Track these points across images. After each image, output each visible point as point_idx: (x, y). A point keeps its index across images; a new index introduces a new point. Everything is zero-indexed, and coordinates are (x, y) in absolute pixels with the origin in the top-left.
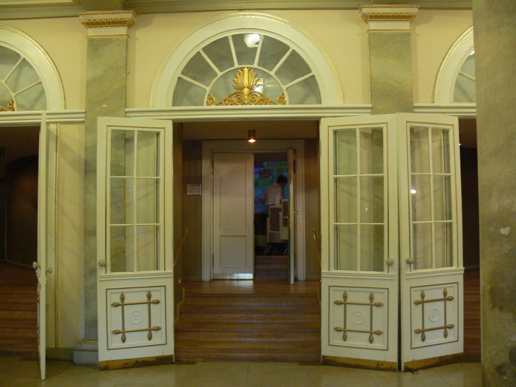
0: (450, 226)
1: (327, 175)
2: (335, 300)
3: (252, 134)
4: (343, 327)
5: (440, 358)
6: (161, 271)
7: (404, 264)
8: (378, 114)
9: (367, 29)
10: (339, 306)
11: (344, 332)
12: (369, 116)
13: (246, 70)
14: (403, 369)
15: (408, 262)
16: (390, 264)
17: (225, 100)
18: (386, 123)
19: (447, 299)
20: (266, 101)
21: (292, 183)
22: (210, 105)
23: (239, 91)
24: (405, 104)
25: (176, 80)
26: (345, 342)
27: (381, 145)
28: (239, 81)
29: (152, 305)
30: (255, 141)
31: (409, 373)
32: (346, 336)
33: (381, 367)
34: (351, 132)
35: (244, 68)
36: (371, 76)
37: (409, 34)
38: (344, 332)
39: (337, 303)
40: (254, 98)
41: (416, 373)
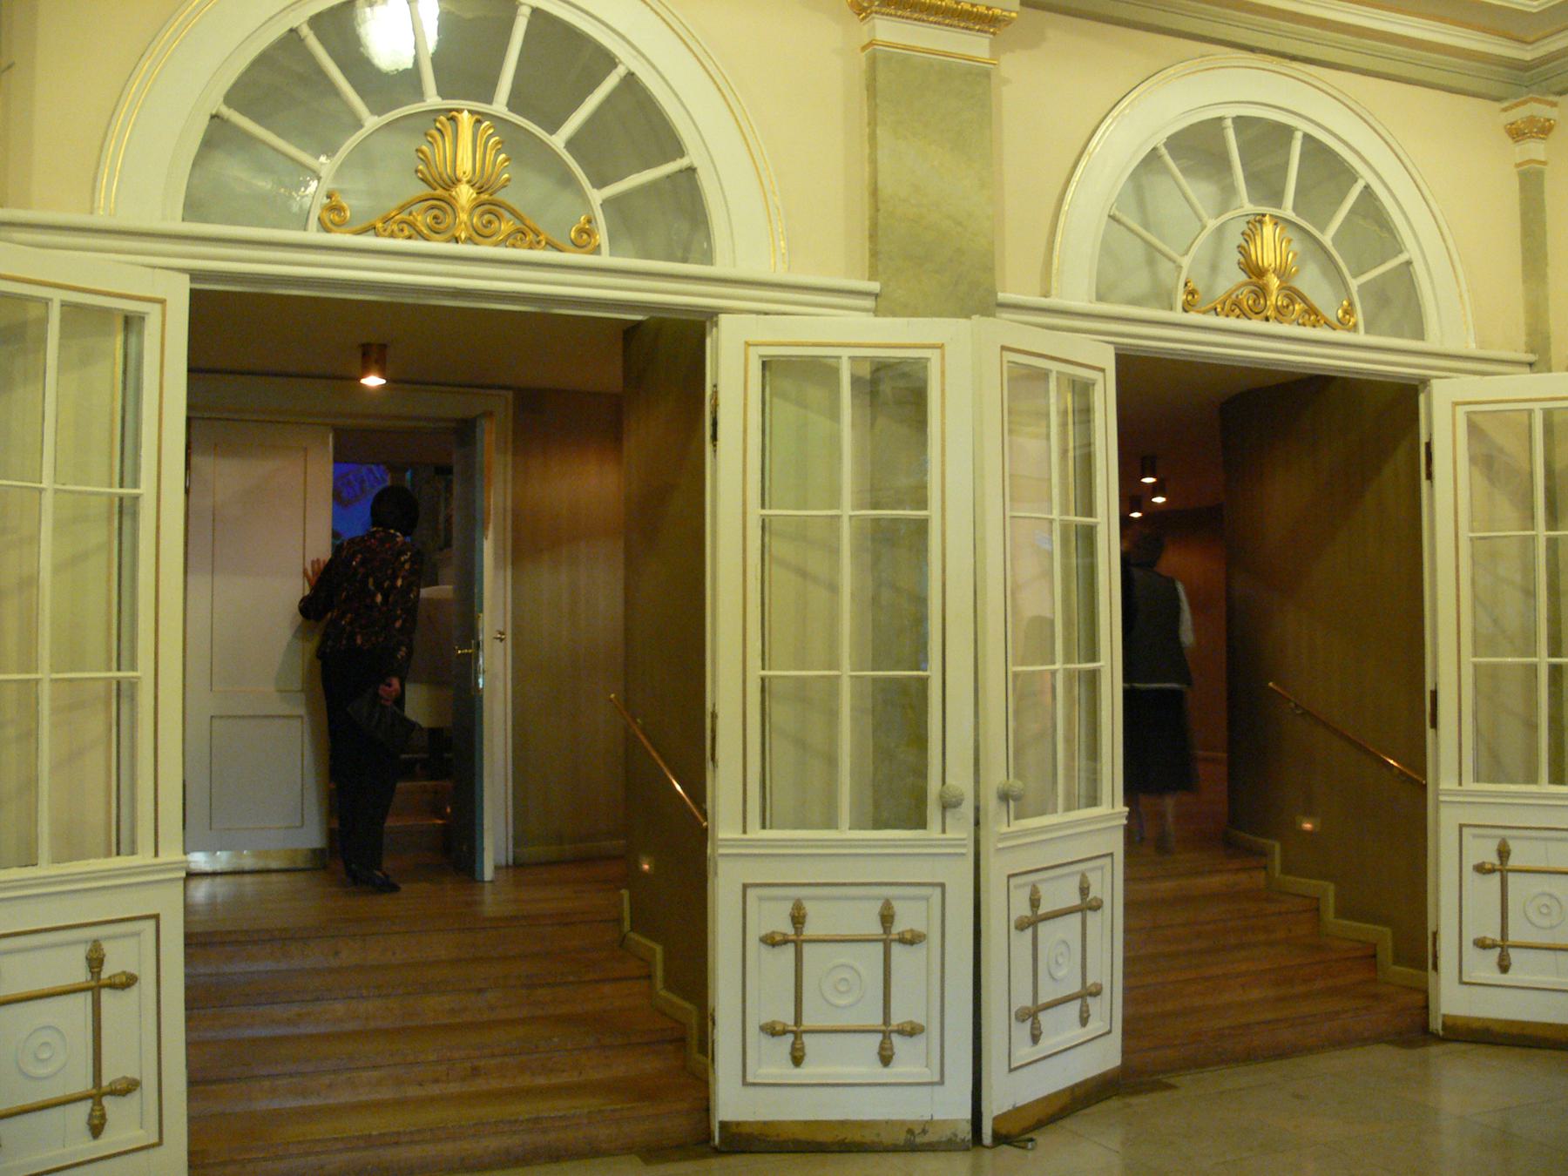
0: (1092, 678)
1: (740, 510)
2: (763, 932)
3: (372, 356)
4: (789, 1021)
5: (1072, 1089)
6: (144, 858)
7: (991, 803)
8: (894, 315)
9: (866, 41)
10: (777, 950)
11: (794, 1038)
12: (869, 319)
13: (466, 119)
14: (987, 1137)
15: (1005, 797)
16: (947, 805)
17: (386, 220)
18: (941, 347)
19: (1088, 906)
20: (531, 236)
21: (490, 534)
22: (327, 230)
23: (440, 192)
24: (976, 297)
25: (204, 122)
26: (798, 1071)
27: (920, 422)
28: (440, 152)
29: (106, 996)
30: (363, 381)
31: (1005, 1147)
32: (802, 1049)
33: (919, 1140)
34: (817, 370)
35: (460, 111)
36: (874, 192)
37: (987, 75)
38: (794, 1038)
39: (771, 941)
40: (490, 222)
41: (1030, 1145)
